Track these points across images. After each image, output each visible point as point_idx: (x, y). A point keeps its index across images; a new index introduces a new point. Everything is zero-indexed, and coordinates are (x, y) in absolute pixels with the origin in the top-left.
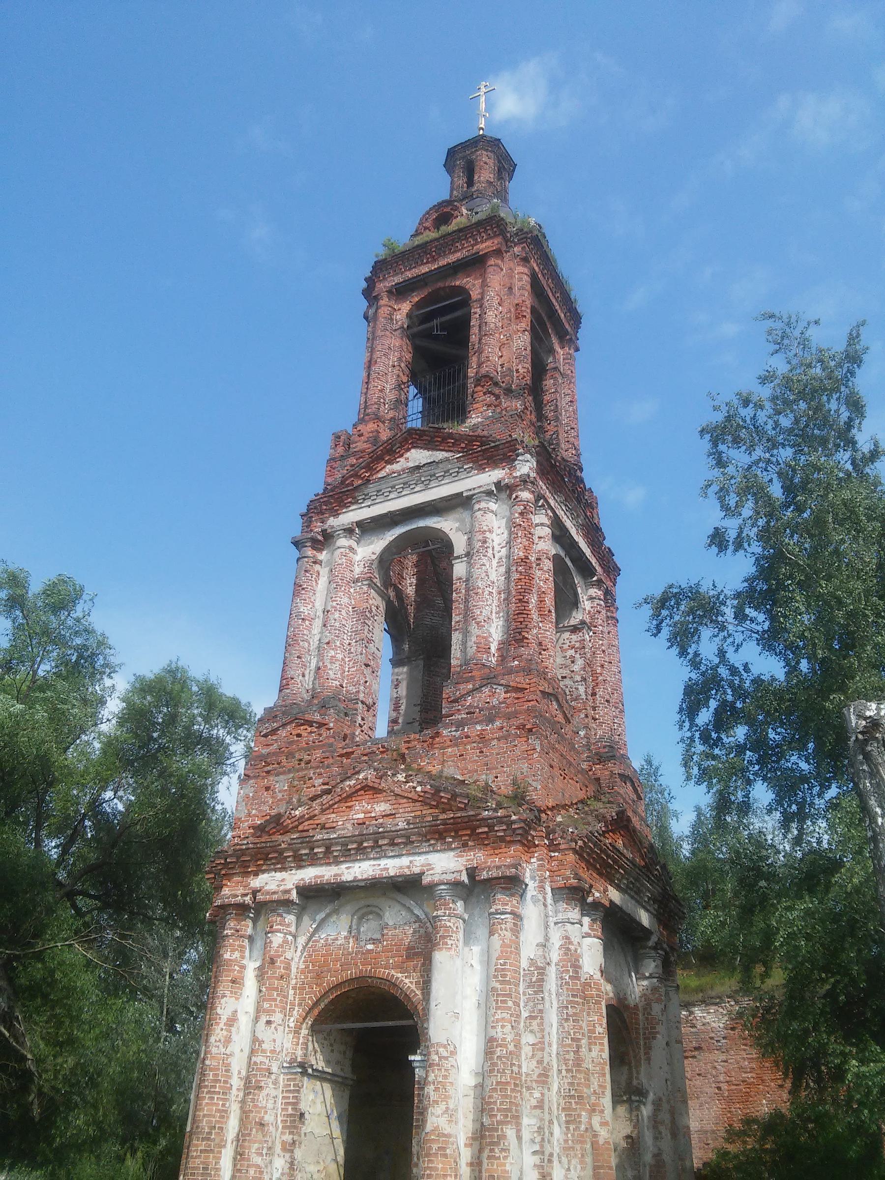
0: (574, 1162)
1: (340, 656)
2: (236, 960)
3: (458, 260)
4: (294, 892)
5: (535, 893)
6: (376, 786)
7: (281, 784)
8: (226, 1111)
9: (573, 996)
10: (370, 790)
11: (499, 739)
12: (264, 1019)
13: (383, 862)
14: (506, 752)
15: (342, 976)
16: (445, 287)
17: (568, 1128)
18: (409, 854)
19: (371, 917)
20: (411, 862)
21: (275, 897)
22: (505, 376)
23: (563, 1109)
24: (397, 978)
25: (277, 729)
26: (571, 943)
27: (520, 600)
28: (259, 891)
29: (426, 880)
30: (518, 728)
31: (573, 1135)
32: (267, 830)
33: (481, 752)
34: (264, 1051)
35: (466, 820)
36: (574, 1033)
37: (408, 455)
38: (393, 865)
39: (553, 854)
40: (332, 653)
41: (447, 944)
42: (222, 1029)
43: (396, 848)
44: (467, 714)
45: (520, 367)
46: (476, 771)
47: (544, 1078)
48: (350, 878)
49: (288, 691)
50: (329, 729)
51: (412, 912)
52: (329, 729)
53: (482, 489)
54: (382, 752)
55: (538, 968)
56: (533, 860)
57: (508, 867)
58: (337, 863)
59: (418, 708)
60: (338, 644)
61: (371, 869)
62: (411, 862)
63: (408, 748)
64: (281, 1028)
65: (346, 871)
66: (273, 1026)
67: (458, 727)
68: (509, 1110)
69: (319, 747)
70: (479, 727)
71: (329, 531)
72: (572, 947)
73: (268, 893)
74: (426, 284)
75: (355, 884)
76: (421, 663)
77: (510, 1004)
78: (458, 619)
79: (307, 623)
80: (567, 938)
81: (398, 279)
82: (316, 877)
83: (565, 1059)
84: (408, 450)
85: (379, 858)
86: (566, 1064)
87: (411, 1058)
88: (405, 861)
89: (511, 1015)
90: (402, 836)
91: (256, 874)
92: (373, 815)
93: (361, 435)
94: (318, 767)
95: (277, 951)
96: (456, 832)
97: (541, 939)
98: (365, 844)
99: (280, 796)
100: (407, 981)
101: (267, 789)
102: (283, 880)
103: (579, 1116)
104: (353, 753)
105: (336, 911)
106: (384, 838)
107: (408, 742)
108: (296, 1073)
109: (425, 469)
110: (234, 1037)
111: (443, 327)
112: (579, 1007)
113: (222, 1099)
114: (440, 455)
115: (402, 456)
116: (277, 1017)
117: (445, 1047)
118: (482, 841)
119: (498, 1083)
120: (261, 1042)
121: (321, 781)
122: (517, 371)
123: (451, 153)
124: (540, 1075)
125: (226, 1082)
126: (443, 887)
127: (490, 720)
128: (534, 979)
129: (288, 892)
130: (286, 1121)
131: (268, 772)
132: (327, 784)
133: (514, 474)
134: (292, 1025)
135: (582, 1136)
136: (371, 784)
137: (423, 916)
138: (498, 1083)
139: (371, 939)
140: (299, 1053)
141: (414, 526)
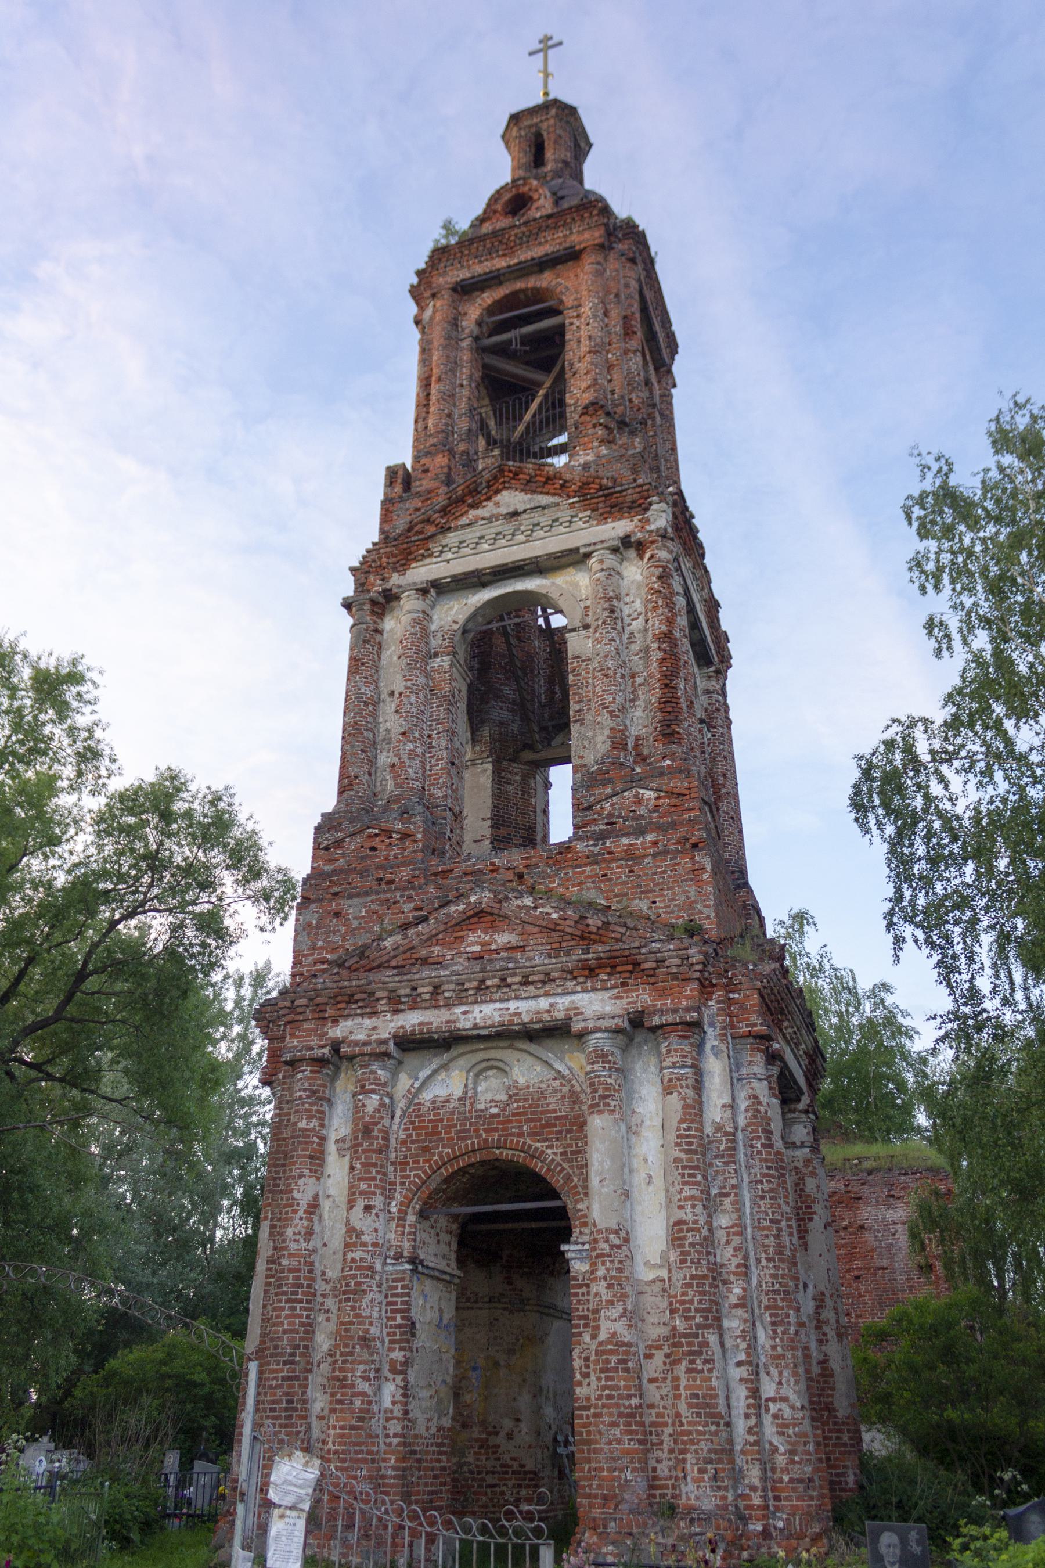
0: (785, 1373)
1: (419, 751)
2: (313, 1130)
3: (547, 255)
4: (391, 1043)
5: (716, 1043)
6: (496, 911)
7: (355, 909)
8: (310, 1325)
9: (769, 1168)
10: (478, 916)
11: (654, 856)
12: (361, 1204)
13: (512, 1005)
14: (665, 872)
15: (460, 1148)
16: (527, 289)
17: (775, 1332)
18: (547, 994)
19: (490, 1073)
20: (551, 1005)
21: (368, 1049)
22: (617, 406)
23: (767, 1308)
24: (537, 1149)
25: (343, 840)
26: (760, 1103)
27: (666, 685)
28: (343, 1042)
29: (577, 1026)
30: (678, 842)
31: (782, 1340)
32: (347, 964)
33: (632, 871)
34: (364, 1244)
35: (627, 953)
36: (773, 1213)
37: (498, 498)
38: (527, 1008)
39: (731, 996)
40: (411, 746)
41: (608, 1105)
42: (301, 1219)
43: (531, 988)
44: (607, 824)
45: (633, 396)
46: (626, 894)
47: (744, 1269)
48: (468, 1025)
49: (352, 793)
50: (416, 841)
51: (551, 1066)
52: (416, 841)
53: (605, 545)
54: (492, 871)
55: (726, 1134)
56: (710, 1003)
57: (688, 1010)
58: (448, 1006)
59: (488, 823)
60: (417, 735)
61: (496, 1014)
62: (551, 1005)
63: (527, 866)
64: (382, 1215)
65: (462, 1017)
66: (374, 1212)
67: (597, 840)
68: (709, 1310)
69: (405, 864)
70: (625, 841)
71: (395, 590)
72: (762, 1109)
73: (356, 1043)
74: (501, 283)
75: (475, 1032)
76: (489, 767)
77: (699, 1178)
78: (578, 707)
79: (371, 708)
80: (756, 1097)
81: (464, 274)
82: (420, 1024)
83: (764, 1246)
84: (498, 492)
85: (508, 1000)
86: (766, 1252)
87: (564, 1247)
88: (543, 1003)
89: (702, 1192)
90: (539, 973)
91: (335, 1021)
92: (493, 947)
93: (426, 471)
94: (405, 889)
95: (372, 1117)
96: (613, 967)
97: (727, 1099)
98: (489, 983)
99: (355, 924)
100: (549, 1151)
101: (337, 914)
102: (374, 1028)
103: (788, 1316)
104: (451, 871)
105: (445, 1067)
106: (515, 974)
107: (527, 858)
108: (404, 1272)
109: (524, 516)
110: (317, 1229)
111: (525, 340)
112: (775, 1181)
113: (306, 1309)
114: (544, 500)
115: (489, 499)
116: (378, 1201)
117: (616, 1232)
118: (650, 977)
119: (693, 1277)
120: (359, 1234)
121: (412, 905)
122: (630, 401)
123: (515, 119)
124: (738, 1266)
125: (309, 1286)
126: (599, 1035)
127: (641, 832)
128: (722, 1148)
129: (385, 1042)
130: (395, 1334)
131: (336, 894)
132: (421, 909)
133: (648, 528)
134: (394, 1210)
135: (792, 1340)
136: (489, 910)
137: (566, 1072)
138: (693, 1277)
139: (492, 1101)
140: (406, 1245)
141: (509, 589)
